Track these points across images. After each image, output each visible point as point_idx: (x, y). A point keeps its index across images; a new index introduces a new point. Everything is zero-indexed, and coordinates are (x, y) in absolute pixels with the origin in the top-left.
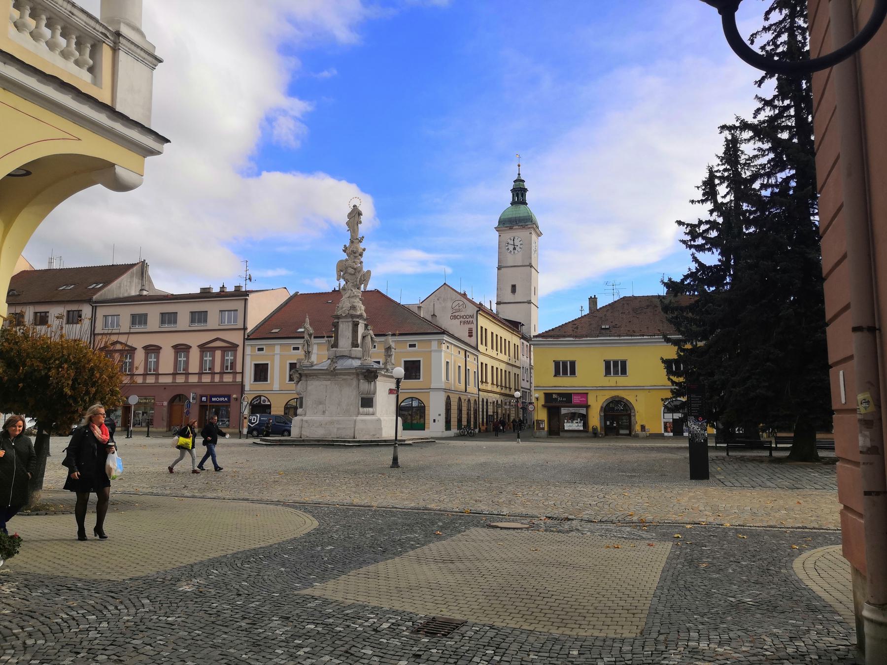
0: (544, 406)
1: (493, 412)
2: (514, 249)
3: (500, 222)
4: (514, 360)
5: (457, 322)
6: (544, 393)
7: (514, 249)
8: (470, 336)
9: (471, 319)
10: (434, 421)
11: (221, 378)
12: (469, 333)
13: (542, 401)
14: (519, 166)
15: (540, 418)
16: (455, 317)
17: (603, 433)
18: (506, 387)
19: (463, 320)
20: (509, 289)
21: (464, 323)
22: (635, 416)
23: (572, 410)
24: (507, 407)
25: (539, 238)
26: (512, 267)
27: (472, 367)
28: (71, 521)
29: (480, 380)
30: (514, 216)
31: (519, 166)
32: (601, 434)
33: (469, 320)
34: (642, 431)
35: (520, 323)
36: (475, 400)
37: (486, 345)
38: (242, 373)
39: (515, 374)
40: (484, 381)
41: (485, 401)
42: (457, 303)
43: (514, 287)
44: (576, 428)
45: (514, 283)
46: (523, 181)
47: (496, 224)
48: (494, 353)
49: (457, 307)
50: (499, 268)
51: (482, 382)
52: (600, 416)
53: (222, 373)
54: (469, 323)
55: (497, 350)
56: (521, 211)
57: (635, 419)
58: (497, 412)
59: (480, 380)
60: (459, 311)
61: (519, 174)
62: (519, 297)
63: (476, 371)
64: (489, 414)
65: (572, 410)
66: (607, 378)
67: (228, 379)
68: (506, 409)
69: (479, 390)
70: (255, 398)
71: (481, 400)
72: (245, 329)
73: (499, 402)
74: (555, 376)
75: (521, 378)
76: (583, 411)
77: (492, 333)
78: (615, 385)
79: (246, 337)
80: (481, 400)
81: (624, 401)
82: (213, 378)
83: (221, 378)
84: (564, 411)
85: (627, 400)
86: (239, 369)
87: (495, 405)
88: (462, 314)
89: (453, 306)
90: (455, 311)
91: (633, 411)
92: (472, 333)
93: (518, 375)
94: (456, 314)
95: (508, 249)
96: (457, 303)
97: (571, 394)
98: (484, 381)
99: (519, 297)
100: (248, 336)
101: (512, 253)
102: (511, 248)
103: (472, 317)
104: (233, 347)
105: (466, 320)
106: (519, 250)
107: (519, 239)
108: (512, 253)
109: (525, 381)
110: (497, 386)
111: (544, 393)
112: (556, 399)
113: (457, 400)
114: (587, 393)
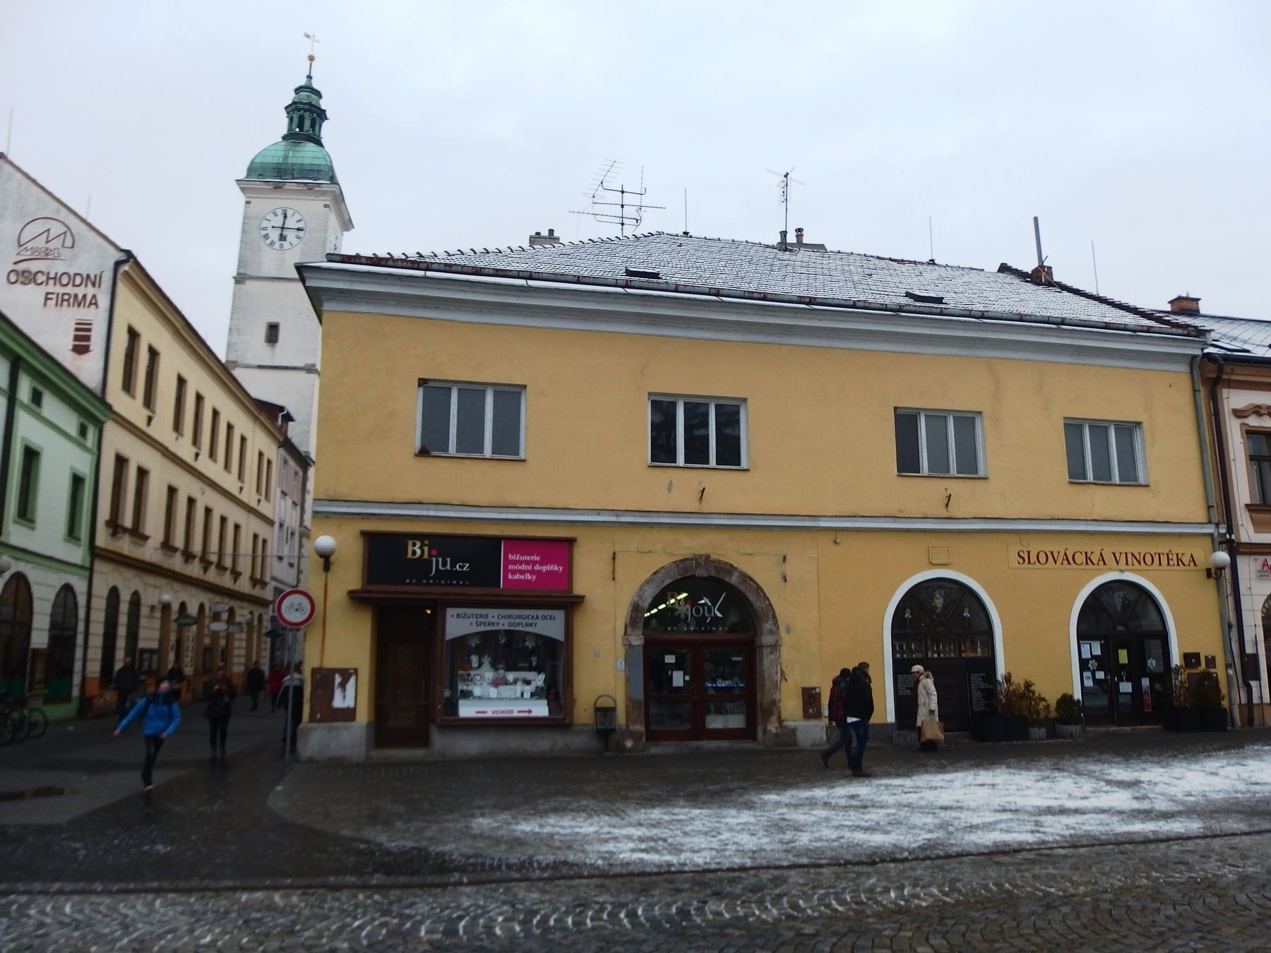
0: (357, 598)
1: (163, 640)
2: (282, 238)
4: (255, 497)
5: (33, 294)
6: (365, 534)
7: (282, 238)
8: (81, 348)
9: (90, 291)
12: (77, 338)
13: (349, 575)
14: (311, 58)
15: (331, 662)
16: (27, 278)
17: (640, 728)
18: (221, 567)
20: (262, 332)
21: (63, 300)
22: (775, 647)
23: (499, 620)
24: (219, 626)
25: (345, 233)
31: (311, 58)
32: (632, 735)
33: (80, 291)
34: (807, 716)
35: (282, 409)
39: (256, 536)
40: (128, 521)
41: (125, 597)
43: (273, 332)
44: (516, 710)
45: (274, 320)
46: (318, 94)
48: (184, 448)
49: (40, 242)
50: (240, 279)
52: (629, 647)
54: (79, 302)
55: (196, 441)
57: (778, 661)
60: (46, 255)
61: (309, 77)
64: (142, 644)
65: (499, 620)
66: (664, 476)
68: (215, 635)
69: (96, 553)
74: (424, 452)
75: (272, 549)
76: (549, 625)
78: (693, 506)
81: (734, 580)
84: (458, 624)
85: (745, 578)
87: (174, 616)
88: (57, 267)
89: (26, 235)
90: (27, 255)
91: (768, 626)
92: (88, 338)
93: (265, 541)
94: (34, 266)
95: (266, 237)
97: (495, 541)
98: (128, 521)
101: (277, 246)
102: (275, 235)
103: (95, 282)
105: (70, 289)
106: (295, 241)
107: (297, 217)
108: (277, 246)
109: (285, 561)
111: (365, 534)
112: (422, 565)
114: (571, 542)
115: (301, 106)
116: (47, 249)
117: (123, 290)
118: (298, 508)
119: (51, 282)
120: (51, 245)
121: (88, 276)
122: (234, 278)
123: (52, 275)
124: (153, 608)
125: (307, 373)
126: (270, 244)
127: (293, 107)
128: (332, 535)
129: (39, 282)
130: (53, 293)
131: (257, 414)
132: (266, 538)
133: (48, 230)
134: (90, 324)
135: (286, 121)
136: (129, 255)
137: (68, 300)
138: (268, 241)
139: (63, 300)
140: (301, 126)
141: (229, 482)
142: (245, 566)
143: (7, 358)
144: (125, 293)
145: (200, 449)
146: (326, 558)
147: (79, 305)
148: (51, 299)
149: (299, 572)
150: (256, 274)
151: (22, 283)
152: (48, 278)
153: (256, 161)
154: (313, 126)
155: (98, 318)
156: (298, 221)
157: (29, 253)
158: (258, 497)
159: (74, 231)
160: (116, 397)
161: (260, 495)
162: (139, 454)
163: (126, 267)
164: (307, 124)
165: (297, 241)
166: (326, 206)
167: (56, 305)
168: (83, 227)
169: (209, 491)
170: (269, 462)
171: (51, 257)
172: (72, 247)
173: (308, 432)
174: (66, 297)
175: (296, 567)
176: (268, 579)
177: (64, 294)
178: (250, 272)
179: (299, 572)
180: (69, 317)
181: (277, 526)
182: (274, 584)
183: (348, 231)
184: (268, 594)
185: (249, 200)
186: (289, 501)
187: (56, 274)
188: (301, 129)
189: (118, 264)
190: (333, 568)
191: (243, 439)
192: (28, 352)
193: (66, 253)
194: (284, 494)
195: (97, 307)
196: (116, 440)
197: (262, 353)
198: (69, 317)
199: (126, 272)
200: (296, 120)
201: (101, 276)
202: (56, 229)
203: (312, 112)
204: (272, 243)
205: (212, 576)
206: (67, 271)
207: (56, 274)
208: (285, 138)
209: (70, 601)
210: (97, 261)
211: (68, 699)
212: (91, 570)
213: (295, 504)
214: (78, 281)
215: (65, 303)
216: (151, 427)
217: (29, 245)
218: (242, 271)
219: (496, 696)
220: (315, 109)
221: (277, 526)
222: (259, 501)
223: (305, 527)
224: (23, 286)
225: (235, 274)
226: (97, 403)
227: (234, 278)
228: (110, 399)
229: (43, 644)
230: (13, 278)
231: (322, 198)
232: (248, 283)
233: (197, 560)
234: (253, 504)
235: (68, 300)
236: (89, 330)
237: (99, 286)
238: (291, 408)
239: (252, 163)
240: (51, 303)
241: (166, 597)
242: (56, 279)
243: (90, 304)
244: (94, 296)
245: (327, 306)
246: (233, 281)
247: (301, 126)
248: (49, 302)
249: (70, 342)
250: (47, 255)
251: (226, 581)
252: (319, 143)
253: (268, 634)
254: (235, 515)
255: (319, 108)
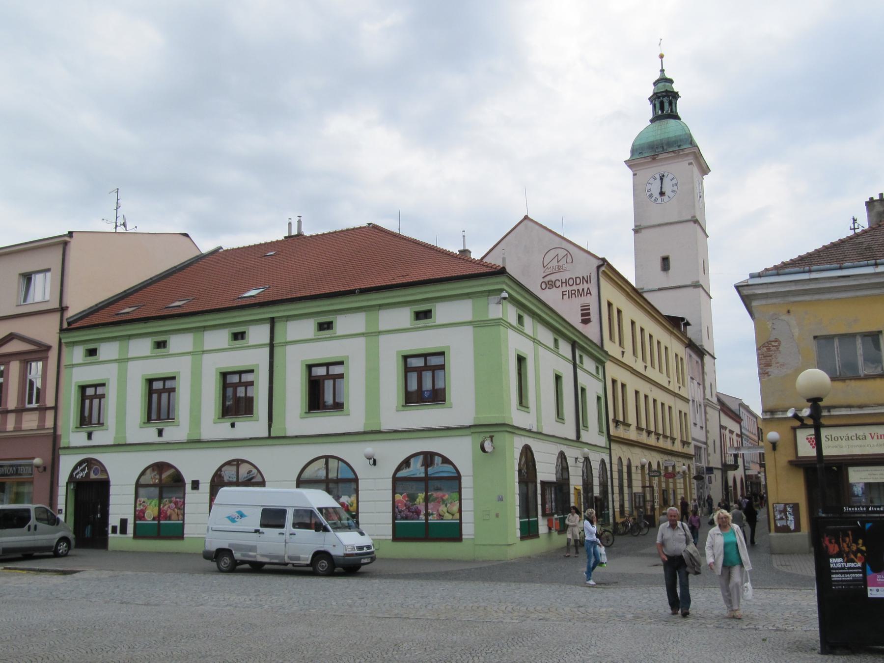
1: (644, 487)
3: (633, 151)
4: (677, 385)
9: (586, 286)
10: (497, 516)
11: (19, 421)
12: (583, 315)
14: (661, 57)
18: (665, 437)
19: (569, 288)
20: (658, 264)
21: (572, 294)
26: (660, 225)
27: (593, 388)
28: (582, 464)
29: (611, 416)
30: (658, 138)
31: (661, 57)
33: (580, 287)
35: (683, 319)
36: (603, 461)
37: (621, 344)
38: (55, 408)
39: (680, 412)
40: (621, 419)
41: (625, 462)
42: (552, 254)
45: (665, 254)
46: (671, 81)
47: (628, 156)
50: (637, 230)
51: (617, 422)
53: (20, 411)
54: (581, 293)
55: (644, 359)
56: (670, 128)
58: (651, 487)
59: (611, 416)
60: (559, 269)
61: (662, 71)
62: (675, 276)
63: (602, 394)
64: (635, 490)
67: (30, 422)
70: (80, 464)
71: (615, 461)
72: (62, 309)
73: (655, 467)
75: (691, 420)
77: (633, 323)
79: (65, 326)
80: (615, 461)
82: (42, 420)
83: (19, 421)
86: (50, 402)
87: (647, 471)
88: (565, 276)
89: (548, 259)
90: (549, 271)
92: (589, 314)
93: (685, 414)
94: (553, 278)
96: (552, 254)
99: (675, 276)
100: (69, 324)
101: (659, 201)
103: (586, 280)
104: (41, 351)
105: (575, 287)
106: (671, 195)
109: (698, 426)
110: (649, 433)
113: (554, 459)
115: (660, 94)
116: (559, 266)
117: (604, 282)
118: (701, 386)
119: (564, 285)
120: (560, 264)
121: (583, 278)
122: (633, 230)
123: (564, 281)
124: (637, 467)
125: (694, 288)
126: (655, 201)
127: (655, 96)
128: (778, 432)
129: (557, 286)
130: (566, 291)
131: (672, 330)
132: (686, 412)
133: (558, 255)
134: (589, 306)
135: (651, 107)
136: (604, 260)
137: (574, 294)
138: (653, 199)
139: (572, 294)
140: (662, 109)
141: (662, 380)
142: (677, 434)
143: (570, 343)
144: (605, 284)
145: (646, 363)
146: (774, 445)
147: (581, 295)
148: (566, 294)
149: (707, 432)
150: (649, 224)
151: (549, 288)
152: (562, 283)
153: (636, 144)
154: (670, 104)
155: (592, 301)
156: (671, 180)
157: (550, 270)
158: (622, 349)
159: (571, 252)
160: (609, 347)
161: (680, 383)
162: (622, 376)
163: (603, 268)
164: (666, 105)
165: (673, 194)
166: (690, 164)
167: (569, 297)
168: (576, 249)
169: (654, 388)
170: (682, 359)
171: (562, 270)
172: (572, 262)
173: (701, 331)
174: (573, 292)
175: (704, 429)
176: (690, 440)
177: (571, 291)
178: (644, 223)
179: (707, 432)
180: (577, 303)
181: (691, 402)
182: (693, 443)
183: (707, 174)
184: (691, 450)
185: (635, 173)
186: (695, 382)
187: (566, 279)
188: (662, 111)
189: (599, 267)
190: (778, 448)
191: (666, 348)
192: (579, 338)
193: (569, 266)
194: (692, 378)
195: (591, 295)
196: (612, 369)
197: (660, 279)
198: (577, 303)
199: (603, 271)
200: (658, 105)
201: (590, 276)
202: (562, 253)
203: (668, 97)
204: (656, 199)
205: (662, 443)
206: (571, 277)
207: (566, 279)
208: (652, 121)
209: (529, 454)
210: (589, 268)
211: (609, 524)
212: (610, 449)
213: (699, 384)
214: (578, 282)
215: (573, 296)
216: (624, 358)
217: (549, 266)
218: (638, 224)
219: (228, 381)
220: (670, 94)
221: (691, 402)
222: (680, 387)
223: (708, 399)
224: (549, 290)
225: (633, 227)
226: (598, 350)
227: (633, 230)
228: (606, 348)
229: (597, 494)
230: (543, 286)
231: (686, 159)
232: (643, 231)
233: (653, 434)
234: (677, 391)
235: (574, 294)
236: (589, 309)
237: (590, 282)
238: (688, 318)
239: (633, 145)
240: (566, 297)
241: (644, 460)
242: (566, 283)
243: (587, 293)
244: (588, 289)
245: (754, 304)
246: (633, 232)
247: (662, 109)
248: (564, 296)
249: (580, 318)
250: (559, 269)
251: (668, 445)
252: (677, 117)
253: (695, 478)
254: (668, 400)
255: (673, 92)
